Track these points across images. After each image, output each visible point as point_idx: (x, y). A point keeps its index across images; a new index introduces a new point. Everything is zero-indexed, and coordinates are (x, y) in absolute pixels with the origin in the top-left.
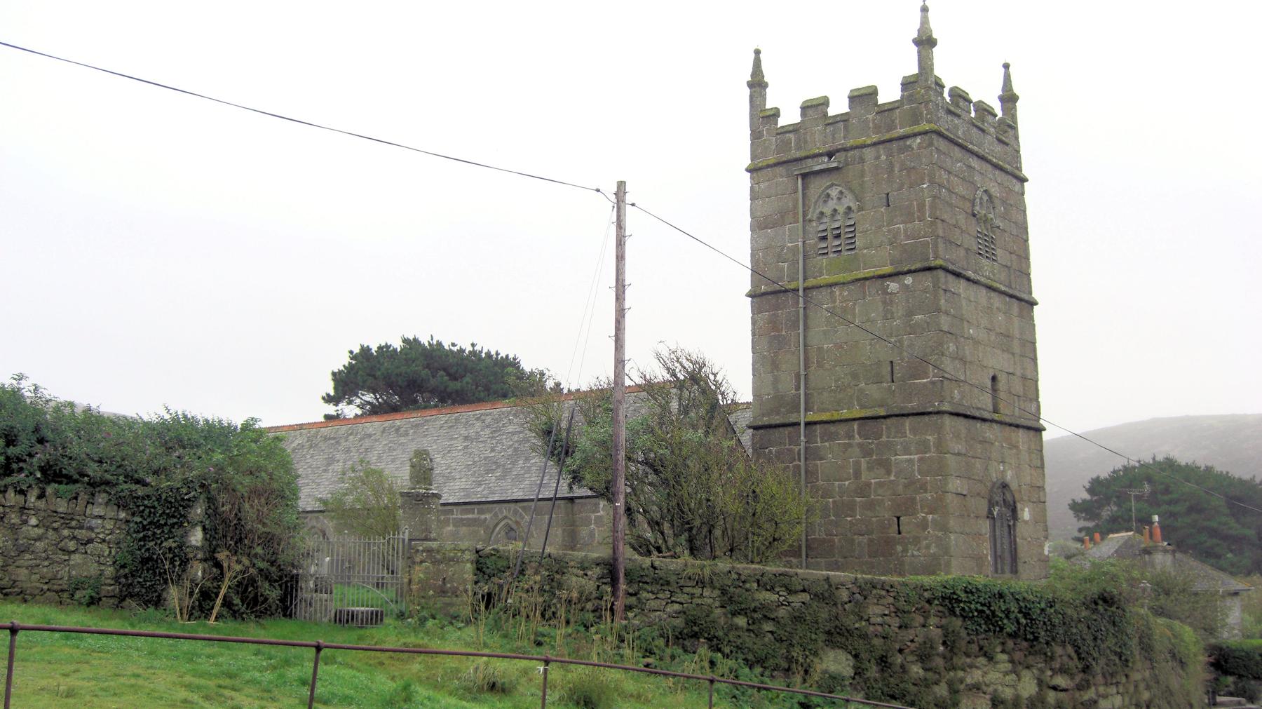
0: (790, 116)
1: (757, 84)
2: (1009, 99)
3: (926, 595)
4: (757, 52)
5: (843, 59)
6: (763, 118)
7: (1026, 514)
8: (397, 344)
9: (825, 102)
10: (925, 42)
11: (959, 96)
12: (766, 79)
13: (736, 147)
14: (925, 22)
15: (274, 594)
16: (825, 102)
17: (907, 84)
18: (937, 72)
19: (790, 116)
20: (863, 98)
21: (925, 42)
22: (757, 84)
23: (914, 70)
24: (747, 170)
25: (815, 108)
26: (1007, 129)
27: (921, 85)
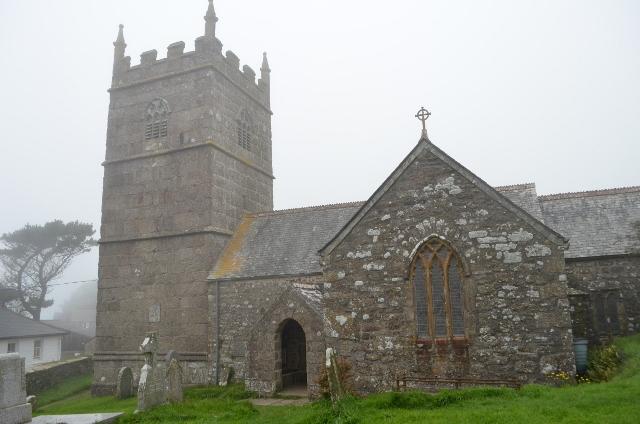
0: (135, 62)
1: (120, 45)
2: (265, 70)
3: (271, 414)
4: (121, 27)
5: (164, 26)
6: (121, 61)
7: (179, 79)
8: (43, 225)
9: (154, 53)
10: (211, 19)
11: (232, 59)
12: (126, 42)
13: (106, 80)
14: (265, 59)
15: (110, 339)
16: (154, 53)
17: (199, 42)
18: (218, 35)
19: (135, 62)
20: (176, 49)
21: (211, 19)
22: (120, 45)
23: (202, 33)
24: (109, 91)
25: (149, 57)
26: (265, 85)
27: (209, 44)
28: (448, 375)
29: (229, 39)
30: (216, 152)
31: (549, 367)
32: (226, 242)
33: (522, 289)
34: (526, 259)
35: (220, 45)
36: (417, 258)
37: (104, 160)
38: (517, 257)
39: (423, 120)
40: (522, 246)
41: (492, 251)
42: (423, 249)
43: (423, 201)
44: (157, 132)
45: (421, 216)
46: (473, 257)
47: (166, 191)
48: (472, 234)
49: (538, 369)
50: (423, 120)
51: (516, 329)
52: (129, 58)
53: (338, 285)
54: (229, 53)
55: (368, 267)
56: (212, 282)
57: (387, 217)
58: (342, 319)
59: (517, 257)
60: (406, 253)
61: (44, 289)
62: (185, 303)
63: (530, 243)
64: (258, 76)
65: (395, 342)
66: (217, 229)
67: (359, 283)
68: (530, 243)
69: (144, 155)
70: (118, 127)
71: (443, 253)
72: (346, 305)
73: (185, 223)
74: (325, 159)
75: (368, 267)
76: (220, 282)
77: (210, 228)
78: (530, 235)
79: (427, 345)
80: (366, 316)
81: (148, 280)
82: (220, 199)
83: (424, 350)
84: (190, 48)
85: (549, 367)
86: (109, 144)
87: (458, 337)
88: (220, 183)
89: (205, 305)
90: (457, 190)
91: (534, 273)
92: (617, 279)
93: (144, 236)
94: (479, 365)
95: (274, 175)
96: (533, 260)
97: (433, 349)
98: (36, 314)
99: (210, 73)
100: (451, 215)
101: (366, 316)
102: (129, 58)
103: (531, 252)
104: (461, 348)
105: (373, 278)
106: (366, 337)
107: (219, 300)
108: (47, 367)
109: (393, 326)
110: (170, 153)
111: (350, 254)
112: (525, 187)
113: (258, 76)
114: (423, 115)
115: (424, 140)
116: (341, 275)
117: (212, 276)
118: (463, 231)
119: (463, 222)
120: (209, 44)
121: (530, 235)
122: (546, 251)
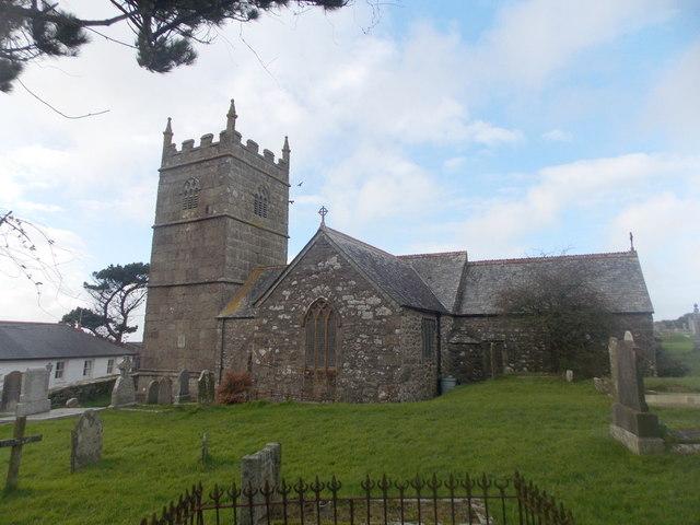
0: (179, 148)
1: (168, 134)
2: (286, 150)
4: (233, 101)
6: (169, 147)
9: (192, 141)
10: (232, 116)
11: (253, 145)
18: (237, 129)
19: (179, 148)
20: (207, 138)
21: (232, 116)
22: (168, 134)
23: (225, 128)
25: (188, 144)
27: (230, 136)
28: (322, 395)
29: (246, 131)
30: (231, 221)
31: (384, 394)
32: (236, 290)
33: (371, 338)
34: (376, 318)
35: (239, 136)
36: (310, 313)
37: (153, 224)
38: (370, 315)
39: (323, 216)
40: (374, 308)
41: (355, 310)
42: (314, 306)
43: (318, 273)
44: (191, 204)
45: (315, 283)
46: (344, 313)
47: (195, 249)
48: (345, 298)
49: (376, 395)
50: (323, 216)
51: (365, 365)
52: (174, 145)
53: (263, 328)
54: (249, 142)
55: (281, 317)
56: (219, 319)
57: (295, 282)
58: (263, 352)
59: (370, 315)
60: (304, 309)
61: (126, 318)
62: (203, 334)
63: (379, 306)
64: (278, 156)
65: (292, 370)
66: (229, 279)
67: (275, 328)
68: (379, 306)
69: (180, 221)
70: (164, 199)
71: (324, 312)
72: (266, 343)
73: (206, 274)
74: (115, 266)
75: (281, 317)
76: (225, 319)
77: (222, 279)
78: (379, 301)
79: (311, 373)
80: (277, 351)
81: (179, 316)
82: (233, 256)
83: (309, 376)
84: (197, 144)
85: (384, 394)
86: (157, 212)
87: (331, 369)
88: (235, 244)
89: (215, 336)
90: (338, 266)
91: (379, 327)
92: (504, 333)
93: (178, 283)
94: (341, 389)
95: (289, 234)
96: (381, 318)
97: (315, 376)
98: (118, 337)
99: (229, 160)
100: (333, 283)
101: (277, 351)
102: (174, 145)
103: (379, 312)
104: (331, 376)
105: (284, 324)
106: (277, 365)
107: (223, 333)
108: (101, 380)
109: (293, 358)
110: (198, 221)
111: (271, 307)
112: (458, 254)
113: (278, 156)
114: (323, 212)
115: (323, 224)
116: (265, 321)
117: (221, 316)
118: (340, 296)
119: (340, 289)
120: (230, 136)
121: (379, 301)
122: (388, 312)
